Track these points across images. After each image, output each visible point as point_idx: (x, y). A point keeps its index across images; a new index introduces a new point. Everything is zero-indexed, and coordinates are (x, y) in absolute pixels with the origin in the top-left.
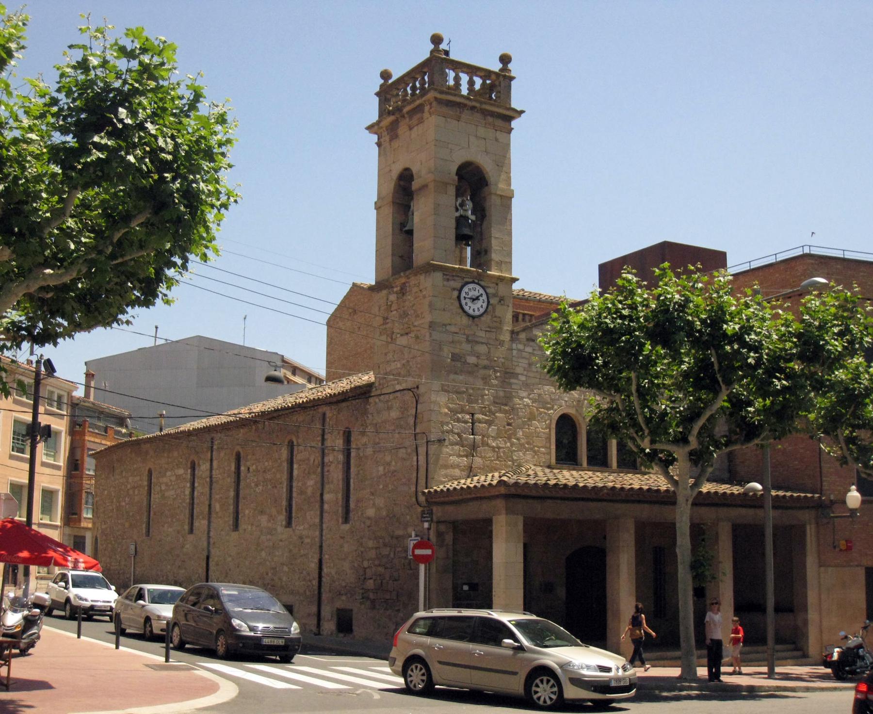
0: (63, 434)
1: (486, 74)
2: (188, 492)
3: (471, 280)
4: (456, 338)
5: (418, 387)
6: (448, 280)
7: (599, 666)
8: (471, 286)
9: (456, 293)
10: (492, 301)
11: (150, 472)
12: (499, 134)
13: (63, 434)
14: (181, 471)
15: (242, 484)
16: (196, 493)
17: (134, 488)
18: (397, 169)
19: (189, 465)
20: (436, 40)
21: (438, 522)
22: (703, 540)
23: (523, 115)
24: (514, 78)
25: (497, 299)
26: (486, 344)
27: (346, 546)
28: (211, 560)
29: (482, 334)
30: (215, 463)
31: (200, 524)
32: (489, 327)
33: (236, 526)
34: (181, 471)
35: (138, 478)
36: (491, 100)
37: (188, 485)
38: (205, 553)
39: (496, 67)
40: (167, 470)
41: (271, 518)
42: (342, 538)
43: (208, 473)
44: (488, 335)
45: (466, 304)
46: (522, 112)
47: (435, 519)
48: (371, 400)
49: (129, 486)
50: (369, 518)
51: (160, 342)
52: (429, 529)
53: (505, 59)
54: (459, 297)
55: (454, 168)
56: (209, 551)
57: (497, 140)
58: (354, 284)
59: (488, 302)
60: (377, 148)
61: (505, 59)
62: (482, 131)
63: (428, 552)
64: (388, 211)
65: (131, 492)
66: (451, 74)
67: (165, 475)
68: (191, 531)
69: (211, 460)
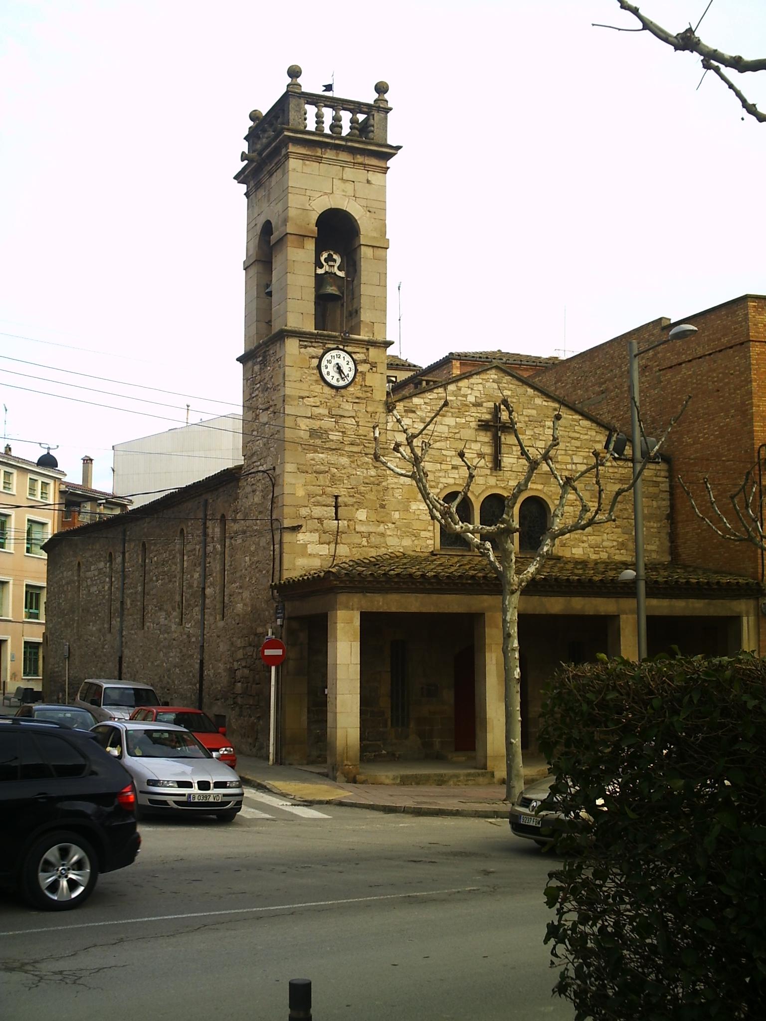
1: (355, 107)
3: (335, 346)
4: (317, 411)
5: (274, 469)
6: (306, 347)
7: (178, 782)
8: (334, 353)
9: (315, 362)
10: (360, 368)
12: (372, 176)
17: (68, 583)
18: (261, 220)
20: (294, 73)
21: (290, 618)
23: (399, 151)
24: (391, 109)
25: (368, 366)
26: (353, 417)
27: (221, 645)
29: (349, 407)
32: (358, 398)
34: (102, 565)
36: (365, 140)
39: (370, 97)
41: (168, 615)
42: (218, 637)
44: (356, 407)
45: (328, 373)
46: (398, 148)
47: (286, 616)
48: (242, 483)
50: (238, 615)
51: (194, 419)
52: (281, 626)
53: (381, 88)
54: (319, 367)
55: (314, 217)
57: (368, 182)
59: (356, 370)
60: (246, 200)
61: (381, 88)
62: (349, 173)
63: (279, 652)
64: (253, 270)
66: (311, 110)
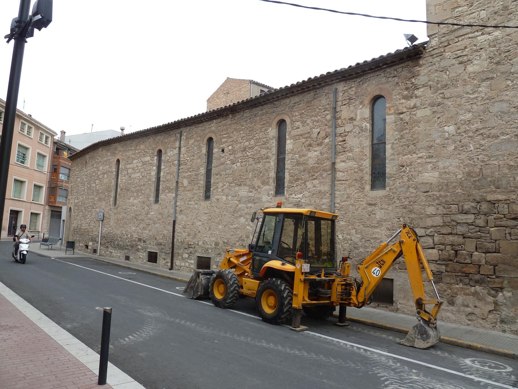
0: (47, 158)
2: (154, 173)
11: (118, 161)
13: (47, 158)
14: (148, 158)
15: (215, 163)
16: (162, 174)
19: (156, 154)
22: (344, 260)
28: (176, 225)
30: (183, 150)
31: (166, 197)
33: (207, 197)
34: (148, 158)
35: (108, 167)
37: (155, 168)
38: (173, 219)
40: (134, 159)
43: (176, 157)
49: (99, 173)
56: (176, 217)
58: (228, 78)
65: (101, 177)
67: (132, 163)
68: (157, 201)
69: (180, 148)
